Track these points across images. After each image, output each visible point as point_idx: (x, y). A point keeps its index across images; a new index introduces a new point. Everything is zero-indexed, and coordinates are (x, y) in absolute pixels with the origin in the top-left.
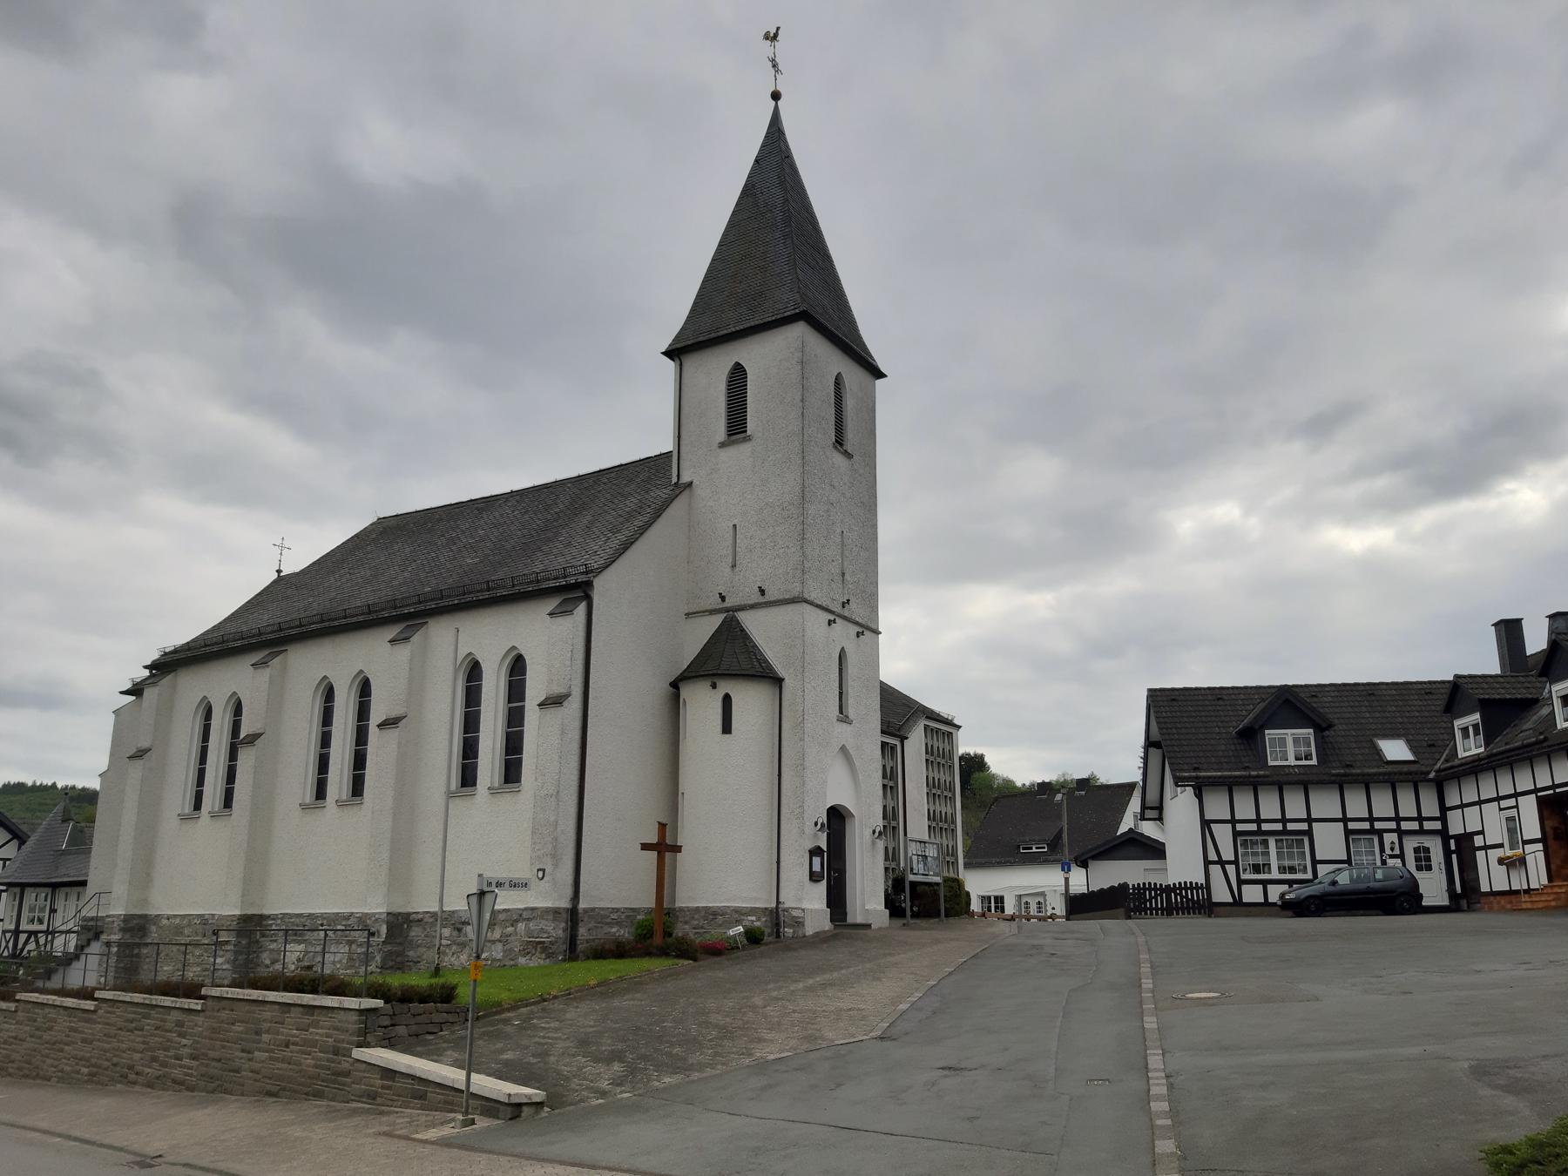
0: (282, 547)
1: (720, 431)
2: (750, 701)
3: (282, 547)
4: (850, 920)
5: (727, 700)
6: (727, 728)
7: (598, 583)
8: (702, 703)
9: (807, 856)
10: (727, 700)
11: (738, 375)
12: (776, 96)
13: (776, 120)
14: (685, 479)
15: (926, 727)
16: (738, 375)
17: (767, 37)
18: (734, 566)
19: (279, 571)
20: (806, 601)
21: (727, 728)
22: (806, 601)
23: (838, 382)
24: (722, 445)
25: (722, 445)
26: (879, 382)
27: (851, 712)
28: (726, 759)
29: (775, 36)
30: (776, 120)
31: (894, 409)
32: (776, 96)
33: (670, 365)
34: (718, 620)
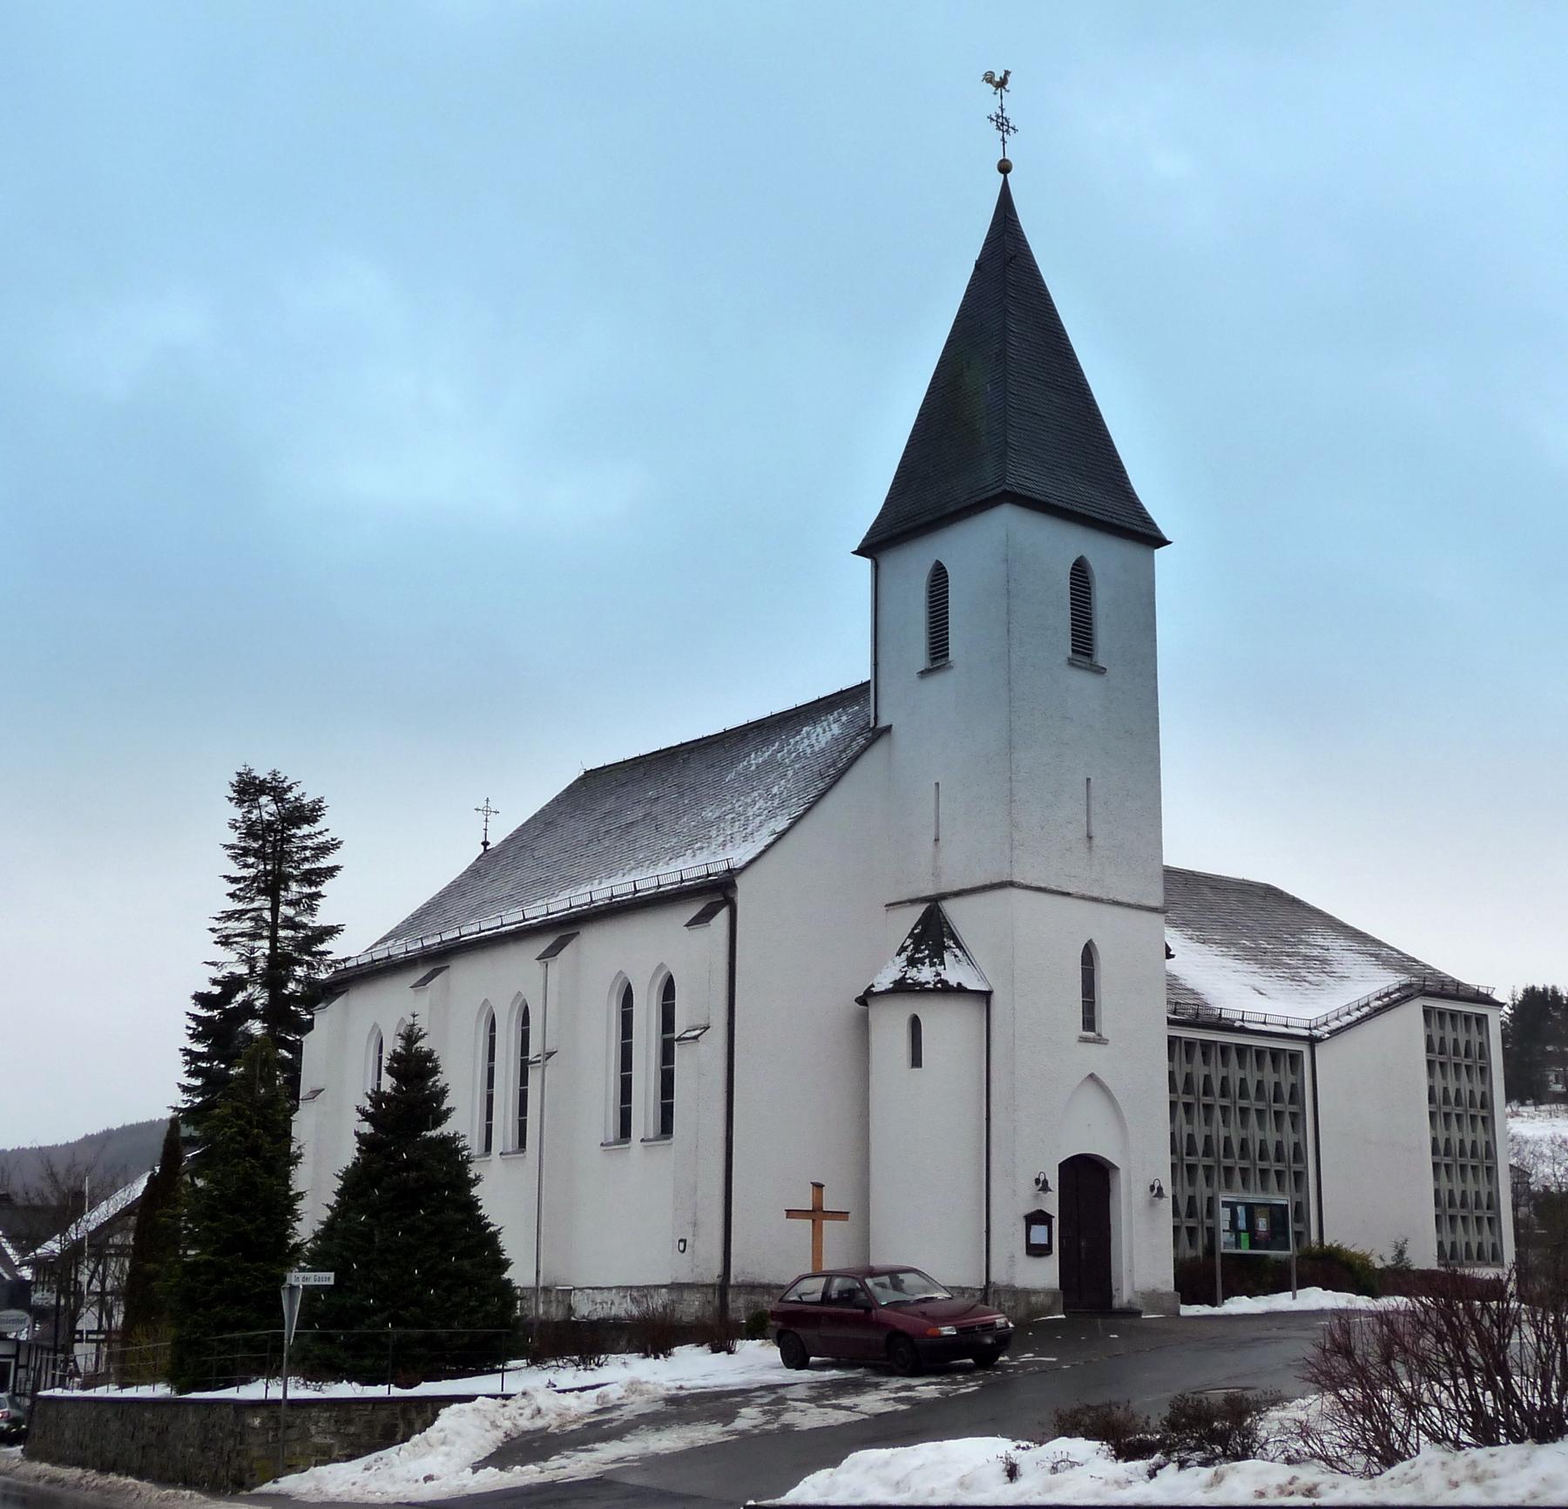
0: (487, 811)
1: (921, 659)
2: (947, 1027)
3: (487, 811)
4: (1116, 1303)
5: (915, 1023)
6: (916, 1061)
7: (739, 881)
8: (890, 1023)
9: (1022, 1225)
10: (915, 1023)
11: (939, 578)
12: (1005, 167)
13: (1005, 204)
14: (883, 723)
15: (1427, 1012)
16: (939, 578)
17: (989, 78)
18: (937, 840)
19: (485, 844)
20: (1012, 884)
21: (916, 1061)
22: (1012, 884)
23: (1080, 574)
24: (924, 673)
25: (924, 673)
26: (1159, 553)
27: (1105, 1024)
28: (924, 1105)
29: (1002, 84)
30: (1005, 204)
31: (1182, 587)
32: (1005, 167)
33: (866, 563)
34: (920, 910)
